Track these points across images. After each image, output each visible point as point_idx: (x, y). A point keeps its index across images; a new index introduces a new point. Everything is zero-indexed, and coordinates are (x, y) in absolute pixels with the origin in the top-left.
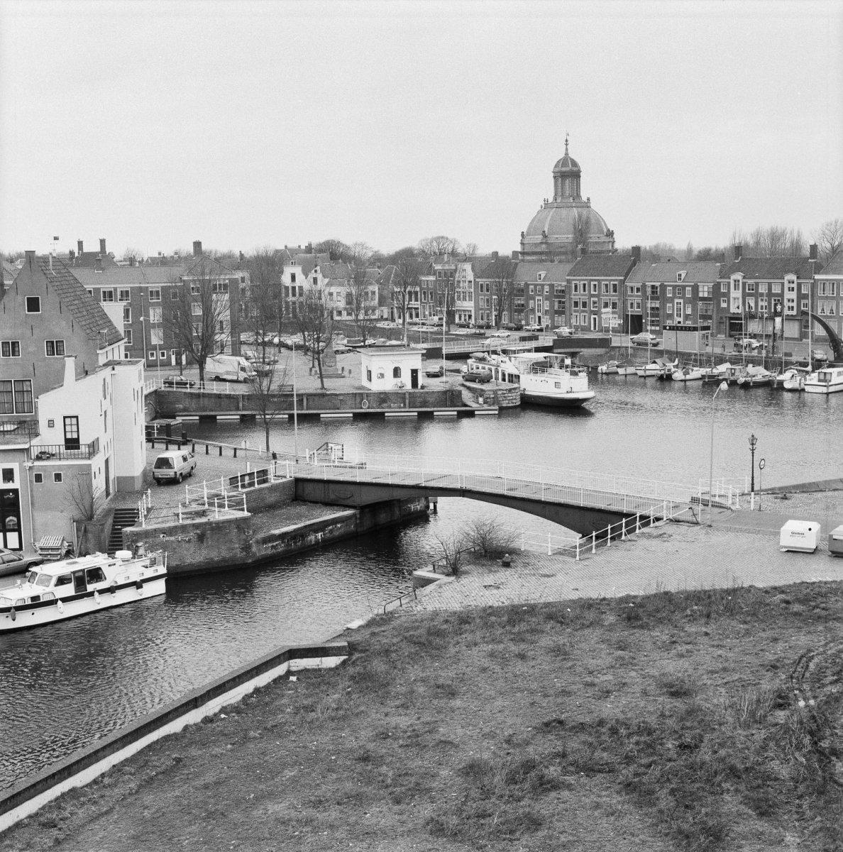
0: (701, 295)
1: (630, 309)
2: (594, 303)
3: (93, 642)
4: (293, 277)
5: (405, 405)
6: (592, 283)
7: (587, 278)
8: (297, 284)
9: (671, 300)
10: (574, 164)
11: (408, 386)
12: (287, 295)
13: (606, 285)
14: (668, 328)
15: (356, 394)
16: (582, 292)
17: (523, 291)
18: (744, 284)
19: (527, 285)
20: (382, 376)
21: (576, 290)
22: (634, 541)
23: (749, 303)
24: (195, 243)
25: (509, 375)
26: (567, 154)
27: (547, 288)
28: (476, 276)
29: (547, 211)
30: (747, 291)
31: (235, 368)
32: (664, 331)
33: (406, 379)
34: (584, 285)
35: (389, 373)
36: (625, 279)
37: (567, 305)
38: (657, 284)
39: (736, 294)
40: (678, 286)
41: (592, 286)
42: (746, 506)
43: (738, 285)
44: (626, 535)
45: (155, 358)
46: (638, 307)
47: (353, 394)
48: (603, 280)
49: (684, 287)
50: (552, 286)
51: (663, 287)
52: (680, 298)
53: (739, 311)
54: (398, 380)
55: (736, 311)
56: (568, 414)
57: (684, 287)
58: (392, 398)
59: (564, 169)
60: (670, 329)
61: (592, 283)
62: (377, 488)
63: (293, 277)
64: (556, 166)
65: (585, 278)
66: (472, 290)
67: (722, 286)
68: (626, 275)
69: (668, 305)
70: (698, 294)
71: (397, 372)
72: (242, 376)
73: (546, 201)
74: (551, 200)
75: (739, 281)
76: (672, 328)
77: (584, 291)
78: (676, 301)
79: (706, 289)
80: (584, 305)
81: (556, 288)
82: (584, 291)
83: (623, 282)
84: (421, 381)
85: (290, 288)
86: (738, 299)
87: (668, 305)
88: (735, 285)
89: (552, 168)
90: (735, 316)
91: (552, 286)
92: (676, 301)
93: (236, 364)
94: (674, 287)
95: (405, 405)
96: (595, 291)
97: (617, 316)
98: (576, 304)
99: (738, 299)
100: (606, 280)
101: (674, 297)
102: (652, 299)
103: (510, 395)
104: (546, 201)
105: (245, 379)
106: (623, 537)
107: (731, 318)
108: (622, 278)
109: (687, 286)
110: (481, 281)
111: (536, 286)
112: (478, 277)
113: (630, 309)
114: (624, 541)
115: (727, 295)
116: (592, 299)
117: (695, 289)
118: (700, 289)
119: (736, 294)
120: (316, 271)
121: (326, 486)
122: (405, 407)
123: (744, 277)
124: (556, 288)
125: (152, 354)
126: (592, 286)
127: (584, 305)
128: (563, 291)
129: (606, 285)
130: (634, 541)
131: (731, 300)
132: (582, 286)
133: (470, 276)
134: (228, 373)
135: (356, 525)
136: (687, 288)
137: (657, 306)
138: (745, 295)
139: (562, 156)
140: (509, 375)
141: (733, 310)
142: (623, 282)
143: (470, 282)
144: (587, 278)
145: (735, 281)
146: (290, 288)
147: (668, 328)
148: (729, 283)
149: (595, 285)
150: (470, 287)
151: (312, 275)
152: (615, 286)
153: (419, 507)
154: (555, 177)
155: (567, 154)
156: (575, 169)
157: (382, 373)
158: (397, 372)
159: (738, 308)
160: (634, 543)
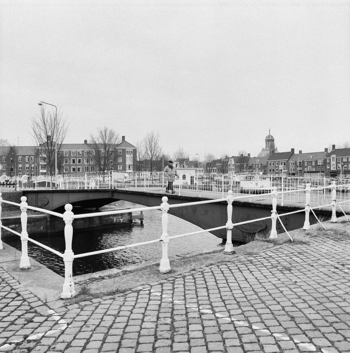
0: (318, 164)
1: (291, 171)
2: (277, 169)
3: (102, 285)
6: (276, 162)
7: (274, 161)
9: (307, 167)
10: (272, 137)
11: (189, 183)
13: (281, 163)
14: (306, 172)
16: (272, 166)
17: (251, 167)
18: (337, 159)
19: (253, 165)
21: (270, 165)
22: (302, 243)
23: (339, 166)
26: (270, 134)
27: (260, 165)
28: (235, 163)
29: (263, 151)
30: (338, 161)
31: (123, 177)
32: (305, 173)
33: (188, 180)
34: (273, 163)
36: (288, 160)
37: (267, 171)
38: (301, 161)
39: (333, 163)
40: (309, 161)
41: (276, 164)
43: (334, 159)
44: (280, 230)
46: (294, 170)
48: (280, 161)
49: (312, 162)
50: (261, 164)
51: (303, 162)
52: (310, 166)
53: (335, 169)
55: (334, 169)
57: (312, 162)
59: (269, 139)
60: (307, 173)
61: (276, 162)
62: (63, 194)
64: (266, 138)
65: (273, 161)
66: (234, 168)
67: (327, 160)
68: (289, 159)
69: (305, 169)
70: (317, 164)
71: (184, 177)
72: (125, 180)
73: (263, 149)
74: (264, 148)
75: (334, 158)
76: (308, 172)
77: (273, 165)
78: (309, 167)
79: (321, 162)
80: (273, 170)
81: (263, 165)
82: (273, 165)
83: (288, 161)
86: (334, 165)
87: (305, 169)
88: (333, 159)
89: (265, 138)
90: (333, 171)
91: (261, 164)
92: (309, 167)
94: (308, 162)
96: (277, 165)
97: (285, 174)
98: (270, 170)
99: (334, 165)
100: (282, 161)
101: (308, 165)
102: (300, 167)
104: (263, 149)
106: (273, 234)
107: (331, 172)
108: (287, 160)
109: (313, 161)
110: (237, 164)
111: (256, 165)
112: (236, 163)
113: (291, 171)
114: (275, 242)
115: (330, 163)
116: (276, 168)
117: (316, 162)
118: (318, 162)
119: (333, 163)
121: (37, 195)
123: (336, 156)
124: (263, 165)
126: (276, 164)
127: (273, 170)
128: (266, 166)
129: (281, 163)
130: (302, 243)
131: (331, 165)
132: (272, 164)
133: (233, 162)
135: (46, 227)
136: (313, 162)
137: (301, 169)
138: (337, 163)
139: (268, 134)
141: (332, 169)
142: (288, 161)
144: (274, 161)
145: (333, 158)
147: (306, 172)
148: (330, 159)
149: (277, 163)
150: (233, 167)
152: (285, 163)
153: (121, 220)
154: (266, 141)
155: (270, 134)
156: (272, 139)
158: (184, 177)
159: (334, 168)
160: (303, 248)
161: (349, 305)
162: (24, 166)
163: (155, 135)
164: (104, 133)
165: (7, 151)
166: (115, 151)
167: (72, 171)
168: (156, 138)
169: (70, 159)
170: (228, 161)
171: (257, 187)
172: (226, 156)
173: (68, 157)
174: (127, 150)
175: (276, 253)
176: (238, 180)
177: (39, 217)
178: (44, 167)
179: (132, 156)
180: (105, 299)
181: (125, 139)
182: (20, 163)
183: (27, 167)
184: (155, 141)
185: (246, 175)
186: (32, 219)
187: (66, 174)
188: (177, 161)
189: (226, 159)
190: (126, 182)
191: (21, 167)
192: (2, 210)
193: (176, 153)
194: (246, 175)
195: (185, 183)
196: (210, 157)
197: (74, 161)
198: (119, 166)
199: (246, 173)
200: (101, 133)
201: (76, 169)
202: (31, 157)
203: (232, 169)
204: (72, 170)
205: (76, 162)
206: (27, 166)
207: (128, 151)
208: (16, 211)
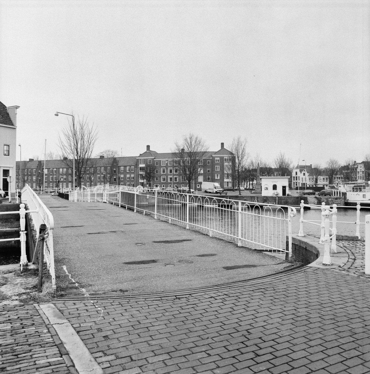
4: (296, 173)
5: (276, 203)
8: (298, 176)
11: (281, 194)
12: (294, 180)
15: (252, 197)
20: (267, 189)
24: (221, 143)
25: (342, 193)
28: (366, 169)
31: (212, 187)
33: (280, 191)
35: (271, 188)
42: (81, 198)
45: (199, 187)
47: (250, 196)
54: (275, 191)
56: (364, 211)
58: (269, 199)
63: (296, 173)
71: (275, 187)
72: (215, 190)
84: (288, 192)
85: (295, 177)
93: (213, 185)
95: (276, 203)
103: (336, 201)
105: (216, 192)
120: (304, 171)
122: (275, 204)
125: (198, 186)
134: (210, 189)
140: (342, 193)
143: (363, 172)
146: (295, 177)
151: (303, 172)
157: (267, 187)
158: (275, 187)
161: (369, 370)
162: (125, 176)
163: (242, 139)
164: (189, 140)
165: (111, 161)
166: (213, 160)
167: (169, 181)
168: (243, 144)
169: (167, 169)
170: (357, 168)
171: (364, 199)
172: (355, 162)
173: (165, 166)
174: (225, 158)
175: (219, 291)
176: (344, 191)
177: (11, 231)
178: (143, 178)
179: (231, 163)
180: (138, 312)
181: (224, 146)
182: (122, 173)
183: (132, 177)
184: (243, 147)
185: (353, 185)
186: (2, 232)
187: (163, 184)
188: (297, 168)
189: (354, 165)
190: (216, 193)
191: (123, 177)
192: (304, 211)
193: (276, 160)
194: (353, 185)
195: (276, 193)
196: (332, 162)
197: (171, 171)
198: (216, 175)
199: (355, 182)
200: (186, 140)
201: (173, 179)
202: (29, 170)
203: (362, 177)
204: (169, 180)
205: (173, 172)
206: (128, 176)
207: (226, 159)
208: (8, 223)
